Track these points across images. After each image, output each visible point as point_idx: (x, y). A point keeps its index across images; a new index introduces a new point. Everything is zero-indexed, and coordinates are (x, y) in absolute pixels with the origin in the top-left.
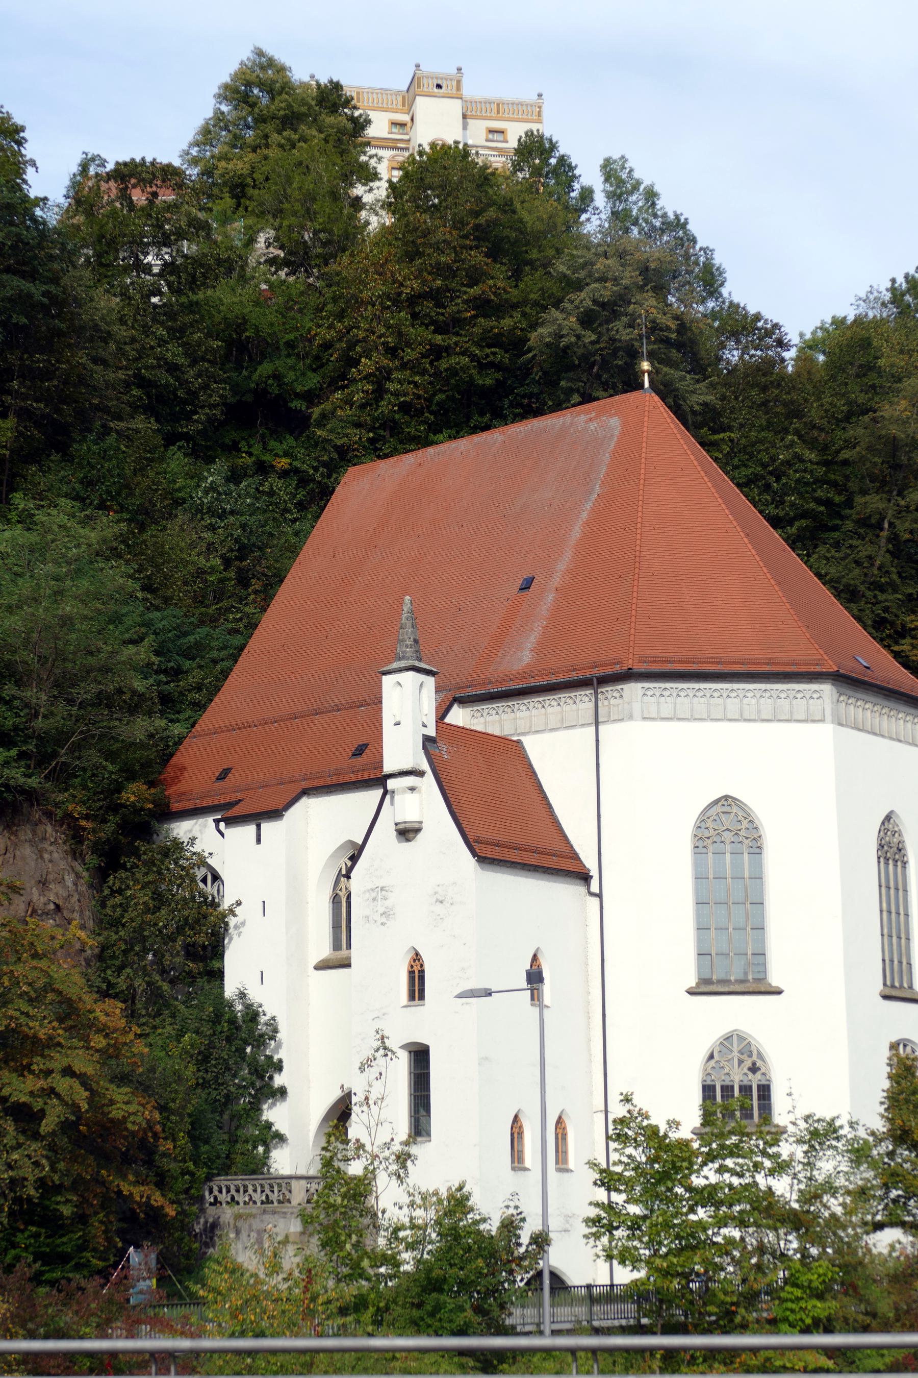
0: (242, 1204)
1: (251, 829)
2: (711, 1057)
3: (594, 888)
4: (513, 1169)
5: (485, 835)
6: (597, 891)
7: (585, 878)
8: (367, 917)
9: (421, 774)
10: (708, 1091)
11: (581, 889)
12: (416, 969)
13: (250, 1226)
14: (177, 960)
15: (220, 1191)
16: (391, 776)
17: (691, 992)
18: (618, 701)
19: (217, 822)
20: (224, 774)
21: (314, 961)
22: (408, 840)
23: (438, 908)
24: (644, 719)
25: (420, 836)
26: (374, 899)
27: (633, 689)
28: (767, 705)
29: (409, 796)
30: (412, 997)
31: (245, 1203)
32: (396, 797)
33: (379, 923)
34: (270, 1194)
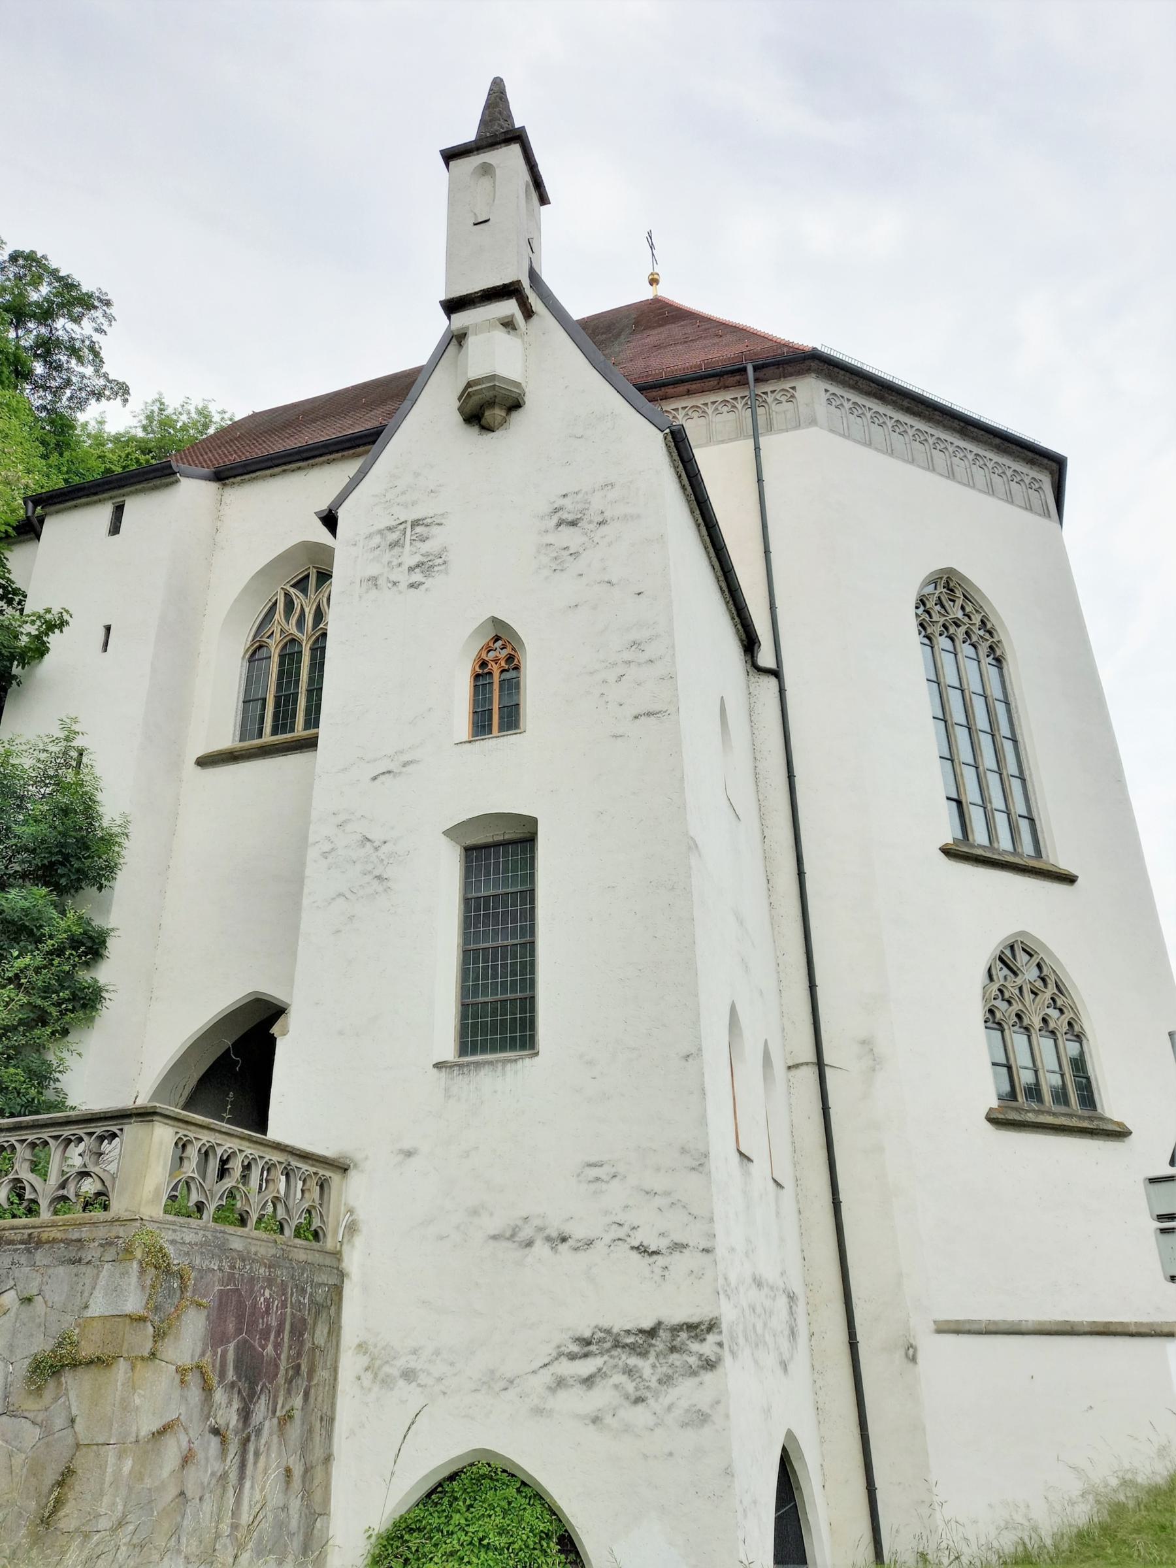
18: (786, 406)
22: (487, 428)
23: (568, 537)
26: (393, 545)
29: (500, 334)
30: (481, 725)
33: (403, 586)
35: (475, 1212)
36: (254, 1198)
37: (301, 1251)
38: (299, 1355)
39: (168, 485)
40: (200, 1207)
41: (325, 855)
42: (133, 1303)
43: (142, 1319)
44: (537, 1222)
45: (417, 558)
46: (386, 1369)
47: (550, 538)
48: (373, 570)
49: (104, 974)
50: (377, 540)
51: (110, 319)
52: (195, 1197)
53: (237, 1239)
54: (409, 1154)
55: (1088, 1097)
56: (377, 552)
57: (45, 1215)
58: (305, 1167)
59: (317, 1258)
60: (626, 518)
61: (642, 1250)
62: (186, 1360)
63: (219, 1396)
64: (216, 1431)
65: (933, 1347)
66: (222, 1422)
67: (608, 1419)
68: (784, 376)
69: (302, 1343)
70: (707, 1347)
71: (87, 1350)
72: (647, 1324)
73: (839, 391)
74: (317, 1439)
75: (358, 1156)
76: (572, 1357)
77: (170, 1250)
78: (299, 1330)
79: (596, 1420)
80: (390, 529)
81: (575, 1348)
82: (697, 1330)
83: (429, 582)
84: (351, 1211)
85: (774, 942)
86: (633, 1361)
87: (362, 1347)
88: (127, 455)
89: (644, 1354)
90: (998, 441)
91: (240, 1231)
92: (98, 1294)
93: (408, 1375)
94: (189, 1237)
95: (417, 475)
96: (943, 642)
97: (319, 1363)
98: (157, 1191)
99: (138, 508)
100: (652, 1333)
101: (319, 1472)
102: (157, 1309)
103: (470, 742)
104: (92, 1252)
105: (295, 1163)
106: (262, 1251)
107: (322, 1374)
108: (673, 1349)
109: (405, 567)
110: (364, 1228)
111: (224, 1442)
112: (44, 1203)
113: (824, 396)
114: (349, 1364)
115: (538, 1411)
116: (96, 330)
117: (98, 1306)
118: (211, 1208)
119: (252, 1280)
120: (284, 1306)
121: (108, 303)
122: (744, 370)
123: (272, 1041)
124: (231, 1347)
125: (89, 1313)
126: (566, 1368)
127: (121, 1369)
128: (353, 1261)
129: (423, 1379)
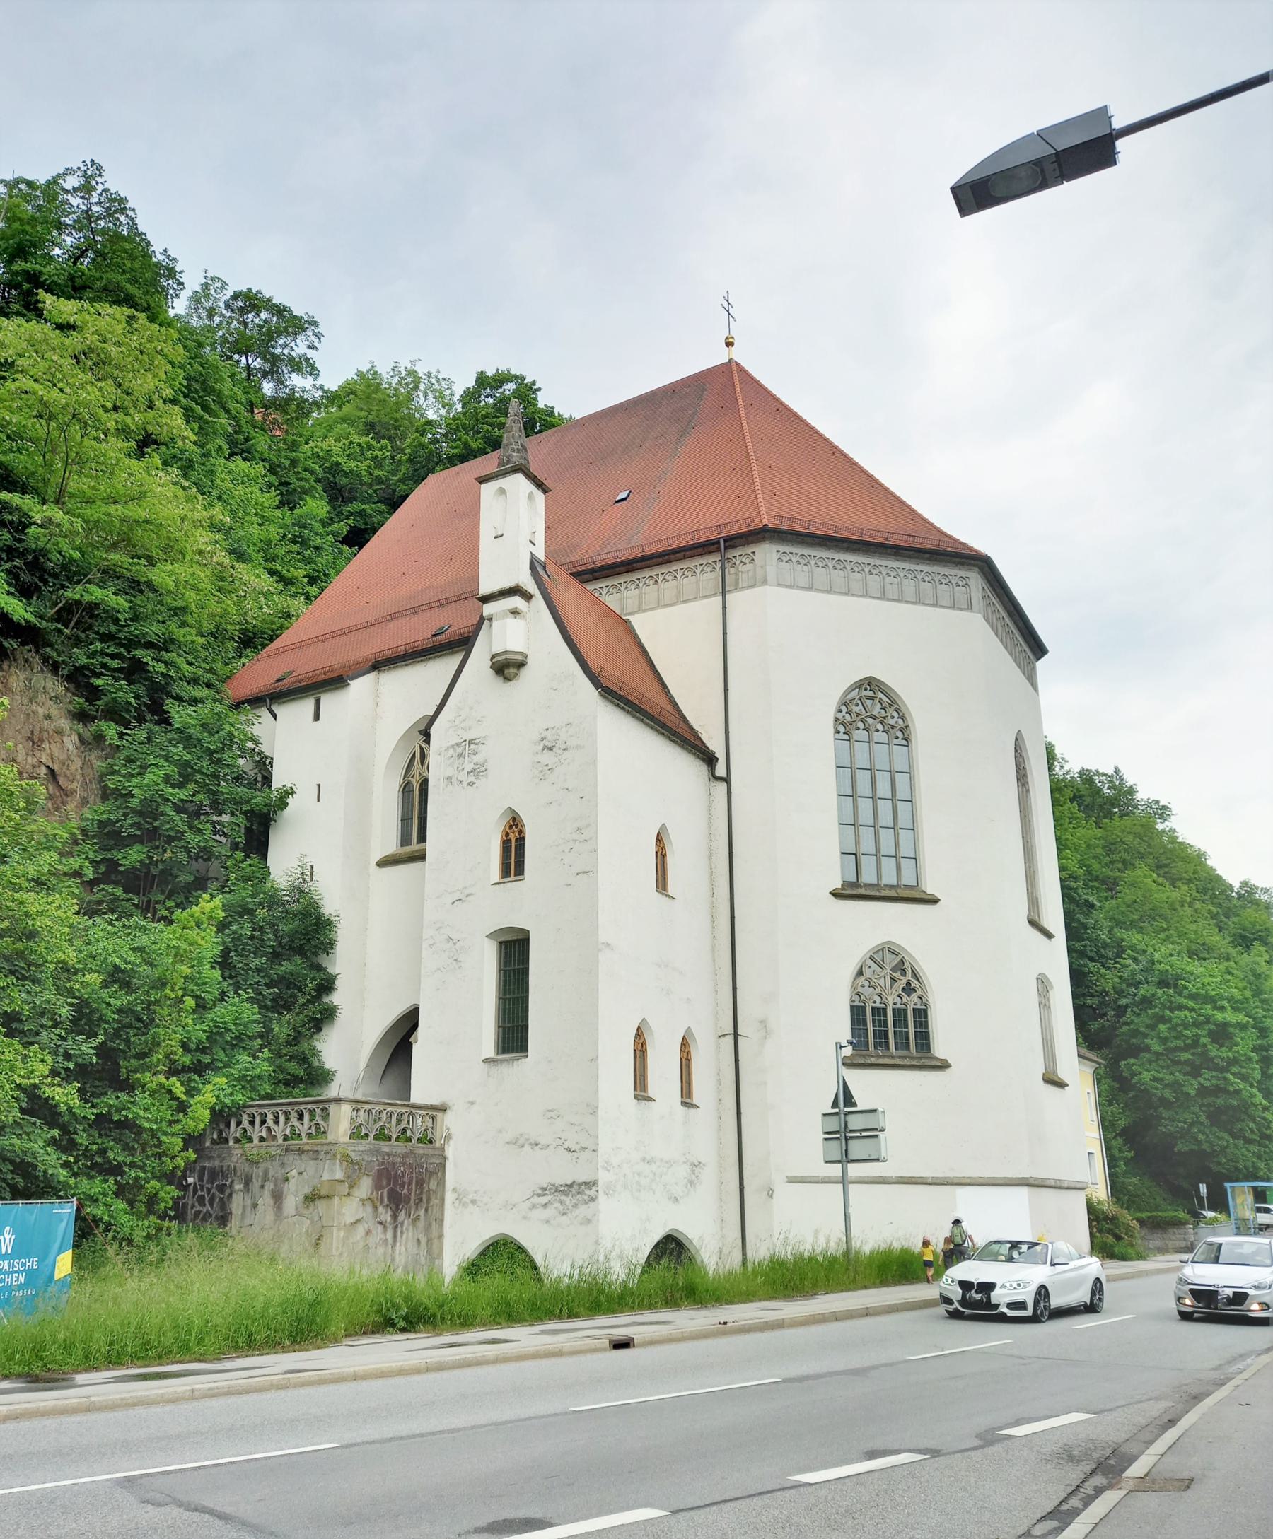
0: (256, 1141)
2: (860, 973)
3: (721, 770)
4: (636, 1097)
6: (724, 775)
7: (709, 759)
8: (449, 778)
10: (857, 1013)
11: (700, 769)
12: (513, 837)
13: (266, 1172)
15: (252, 1123)
17: (836, 894)
18: (749, 566)
21: (377, 857)
22: (507, 679)
23: (547, 758)
24: (779, 585)
25: (524, 672)
26: (460, 756)
27: (767, 553)
28: (909, 587)
29: (511, 621)
30: (506, 872)
31: (262, 1139)
32: (494, 623)
33: (465, 783)
34: (297, 1124)
35: (500, 1131)
36: (394, 1129)
37: (421, 1149)
38: (421, 1193)
39: (343, 687)
40: (367, 1135)
41: (431, 946)
42: (339, 1175)
43: (343, 1181)
44: (526, 1137)
45: (472, 766)
46: (464, 1199)
47: (539, 758)
48: (450, 772)
49: (336, 998)
50: (451, 752)
51: (318, 336)
52: (364, 1131)
53: (385, 1147)
54: (472, 1103)
55: (924, 1039)
56: (451, 760)
57: (305, 1140)
58: (420, 1112)
59: (431, 1152)
60: (578, 747)
61: (569, 1150)
62: (364, 1196)
63: (381, 1209)
64: (381, 1223)
65: (782, 1189)
66: (383, 1220)
67: (552, 1222)
68: (748, 543)
69: (422, 1189)
70: (592, 1193)
71: (323, 1193)
72: (569, 1182)
73: (787, 549)
74: (433, 1228)
75: (450, 1104)
76: (539, 1195)
77: (352, 1154)
78: (420, 1183)
79: (547, 1222)
80: (457, 744)
81: (540, 1192)
82: (589, 1185)
83: (478, 782)
84: (448, 1129)
85: (714, 961)
86: (563, 1198)
87: (454, 1190)
88: (351, 443)
89: (567, 1195)
90: (927, 556)
91: (388, 1143)
92: (326, 1171)
93: (473, 1202)
94: (362, 1148)
95: (471, 708)
96: (860, 735)
97: (433, 1197)
98: (346, 1132)
99: (329, 701)
100: (571, 1186)
101: (436, 1241)
102: (349, 1177)
103: (498, 884)
104: (322, 1156)
105: (414, 1111)
106: (399, 1151)
107: (434, 1201)
108: (579, 1193)
109: (466, 772)
110: (454, 1137)
111: (385, 1227)
112: (303, 1136)
113: (775, 556)
114: (449, 1197)
115: (525, 1218)
116: (309, 347)
117: (326, 1177)
118: (372, 1135)
119: (394, 1164)
120: (412, 1173)
121: (316, 324)
122: (718, 543)
123: (410, 1045)
124: (385, 1191)
125: (323, 1179)
126: (536, 1200)
127: (336, 1200)
128: (449, 1152)
129: (479, 1204)
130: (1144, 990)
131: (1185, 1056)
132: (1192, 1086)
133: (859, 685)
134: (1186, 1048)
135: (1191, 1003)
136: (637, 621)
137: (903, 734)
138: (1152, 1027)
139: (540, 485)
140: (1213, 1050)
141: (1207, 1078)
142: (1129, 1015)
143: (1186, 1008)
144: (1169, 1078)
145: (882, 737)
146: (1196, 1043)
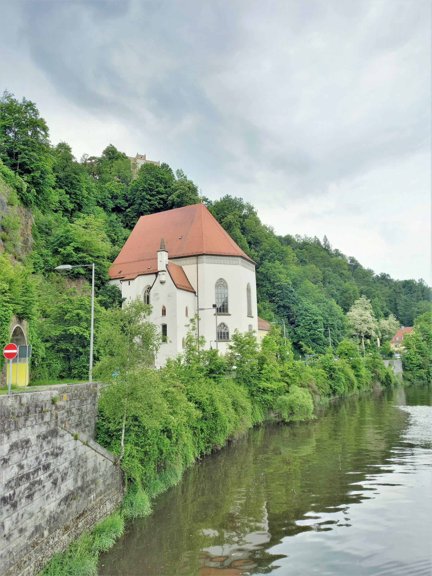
1: (127, 282)
3: (197, 295)
5: (179, 283)
7: (195, 293)
9: (165, 271)
11: (193, 294)
14: (330, 273)
16: (159, 272)
19: (121, 281)
20: (120, 273)
27: (204, 257)
28: (228, 262)
29: (163, 276)
30: (163, 315)
99: (131, 282)
114: (156, 363)
130: (301, 312)
131: (308, 327)
132: (308, 333)
133: (220, 279)
134: (308, 325)
135: (310, 315)
136: (183, 267)
137: (226, 287)
138: (302, 320)
139: (167, 252)
140: (314, 326)
141: (312, 332)
142: (298, 318)
143: (309, 316)
144: (304, 332)
145: (223, 288)
146: (310, 324)
